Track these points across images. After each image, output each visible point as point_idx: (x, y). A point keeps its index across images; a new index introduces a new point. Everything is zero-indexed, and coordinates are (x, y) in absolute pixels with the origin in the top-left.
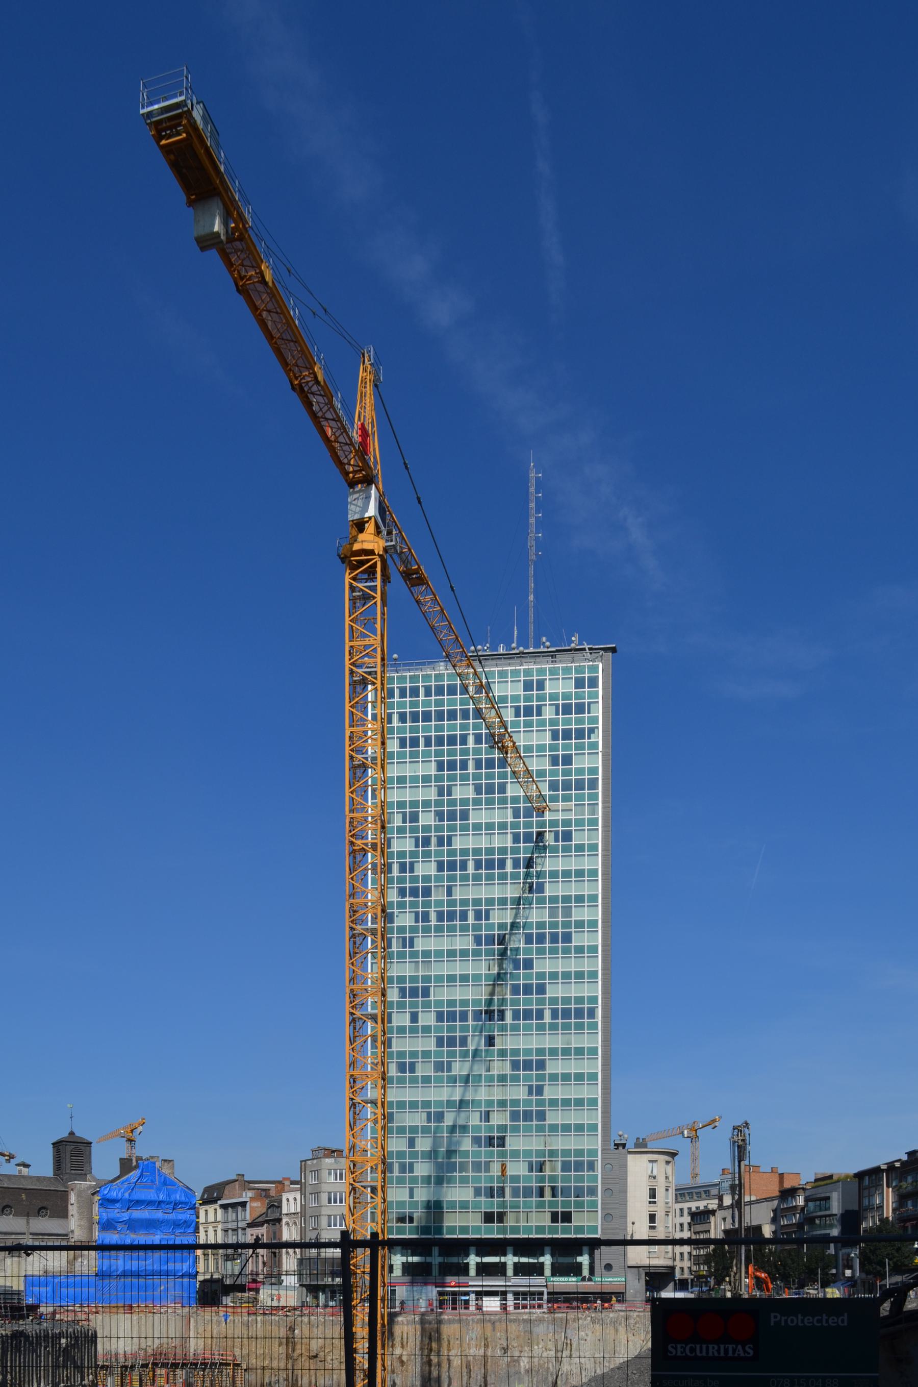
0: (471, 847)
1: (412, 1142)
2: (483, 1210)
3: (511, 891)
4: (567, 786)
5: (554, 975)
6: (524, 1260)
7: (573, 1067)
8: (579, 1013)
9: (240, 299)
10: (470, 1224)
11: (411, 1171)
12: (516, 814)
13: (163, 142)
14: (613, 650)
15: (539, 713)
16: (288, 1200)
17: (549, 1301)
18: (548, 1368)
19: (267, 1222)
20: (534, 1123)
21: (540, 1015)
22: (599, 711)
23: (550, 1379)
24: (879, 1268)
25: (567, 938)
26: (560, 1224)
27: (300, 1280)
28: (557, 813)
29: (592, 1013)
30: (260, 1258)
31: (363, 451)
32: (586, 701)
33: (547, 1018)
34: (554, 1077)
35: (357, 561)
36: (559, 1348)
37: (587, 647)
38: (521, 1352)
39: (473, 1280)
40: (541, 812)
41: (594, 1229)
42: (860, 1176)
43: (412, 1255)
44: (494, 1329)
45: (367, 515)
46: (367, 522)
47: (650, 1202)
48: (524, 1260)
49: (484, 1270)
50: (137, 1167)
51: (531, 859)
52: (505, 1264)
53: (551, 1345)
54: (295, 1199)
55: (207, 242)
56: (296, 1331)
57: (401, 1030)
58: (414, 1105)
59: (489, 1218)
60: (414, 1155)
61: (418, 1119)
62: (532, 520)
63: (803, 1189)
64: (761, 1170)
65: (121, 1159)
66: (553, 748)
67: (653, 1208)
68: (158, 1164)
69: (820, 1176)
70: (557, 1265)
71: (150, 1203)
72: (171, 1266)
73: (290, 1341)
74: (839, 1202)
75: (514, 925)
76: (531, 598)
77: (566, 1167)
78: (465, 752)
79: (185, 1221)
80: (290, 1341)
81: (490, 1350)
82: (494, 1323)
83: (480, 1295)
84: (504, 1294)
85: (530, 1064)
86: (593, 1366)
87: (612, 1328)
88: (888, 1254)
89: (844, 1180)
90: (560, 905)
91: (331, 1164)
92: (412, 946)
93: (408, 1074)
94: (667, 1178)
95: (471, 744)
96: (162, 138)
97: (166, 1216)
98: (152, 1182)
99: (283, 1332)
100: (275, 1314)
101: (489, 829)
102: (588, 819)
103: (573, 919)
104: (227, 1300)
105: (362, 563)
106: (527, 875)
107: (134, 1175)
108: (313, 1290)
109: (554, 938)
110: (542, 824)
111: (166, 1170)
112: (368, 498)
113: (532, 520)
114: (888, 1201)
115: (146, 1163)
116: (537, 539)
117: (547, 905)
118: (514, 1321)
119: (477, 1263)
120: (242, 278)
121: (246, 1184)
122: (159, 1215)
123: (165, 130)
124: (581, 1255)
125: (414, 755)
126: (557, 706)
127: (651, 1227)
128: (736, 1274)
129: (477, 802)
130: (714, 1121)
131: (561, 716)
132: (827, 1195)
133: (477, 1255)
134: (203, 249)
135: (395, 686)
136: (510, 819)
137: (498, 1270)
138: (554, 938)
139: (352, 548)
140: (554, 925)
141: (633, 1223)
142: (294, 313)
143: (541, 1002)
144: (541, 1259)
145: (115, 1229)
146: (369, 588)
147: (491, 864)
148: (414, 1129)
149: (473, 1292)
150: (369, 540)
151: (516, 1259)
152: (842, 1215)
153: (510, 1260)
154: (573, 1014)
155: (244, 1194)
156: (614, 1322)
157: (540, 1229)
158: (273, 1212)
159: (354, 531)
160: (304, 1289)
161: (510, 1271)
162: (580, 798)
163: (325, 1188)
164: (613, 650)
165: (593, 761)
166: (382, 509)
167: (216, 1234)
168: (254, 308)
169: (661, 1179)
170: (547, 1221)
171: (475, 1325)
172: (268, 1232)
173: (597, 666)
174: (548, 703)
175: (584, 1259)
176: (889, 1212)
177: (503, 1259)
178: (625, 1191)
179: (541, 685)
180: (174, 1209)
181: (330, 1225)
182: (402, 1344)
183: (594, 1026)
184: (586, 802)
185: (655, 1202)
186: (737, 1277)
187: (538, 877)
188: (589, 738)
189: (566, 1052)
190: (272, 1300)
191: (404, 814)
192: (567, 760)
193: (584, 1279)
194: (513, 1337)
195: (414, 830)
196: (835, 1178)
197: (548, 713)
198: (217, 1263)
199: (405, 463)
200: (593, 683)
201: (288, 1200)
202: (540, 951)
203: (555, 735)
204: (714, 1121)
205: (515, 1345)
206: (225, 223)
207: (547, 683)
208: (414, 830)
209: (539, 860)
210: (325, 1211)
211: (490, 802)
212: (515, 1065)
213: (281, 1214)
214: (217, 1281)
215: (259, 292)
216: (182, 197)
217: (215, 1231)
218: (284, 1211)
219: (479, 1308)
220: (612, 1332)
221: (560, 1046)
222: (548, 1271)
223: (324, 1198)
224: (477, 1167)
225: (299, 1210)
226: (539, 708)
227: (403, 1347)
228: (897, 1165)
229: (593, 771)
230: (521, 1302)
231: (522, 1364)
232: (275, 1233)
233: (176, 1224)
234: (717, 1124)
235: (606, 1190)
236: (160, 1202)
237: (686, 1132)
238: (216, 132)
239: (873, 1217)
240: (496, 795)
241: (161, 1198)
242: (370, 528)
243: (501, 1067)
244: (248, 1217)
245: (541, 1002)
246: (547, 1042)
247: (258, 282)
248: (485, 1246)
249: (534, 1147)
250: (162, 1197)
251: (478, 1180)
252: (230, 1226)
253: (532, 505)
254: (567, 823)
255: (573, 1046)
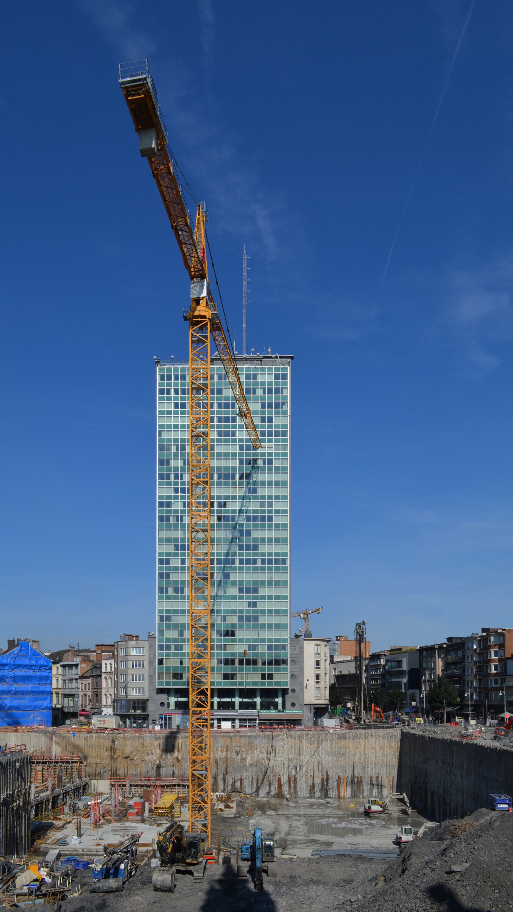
0: (216, 466)
1: (182, 633)
2: (223, 672)
3: (239, 492)
4: (270, 434)
5: (263, 540)
6: (245, 700)
7: (273, 591)
8: (277, 561)
9: (154, 180)
10: (215, 680)
11: (181, 649)
12: (241, 448)
13: (130, 98)
14: (292, 358)
15: (254, 393)
16: (106, 664)
17: (260, 724)
18: (262, 763)
19: (93, 676)
20: (252, 623)
21: (255, 562)
22: (288, 393)
23: (263, 770)
24: (440, 705)
25: (270, 519)
26: (266, 680)
27: (114, 711)
28: (266, 448)
29: (284, 561)
30: (87, 697)
31: (201, 262)
32: (281, 387)
33: (259, 564)
34: (263, 597)
35: (195, 321)
36: (269, 752)
37: (278, 355)
38: (247, 754)
39: (216, 712)
40: (255, 448)
41: (286, 683)
42: (421, 650)
43: (181, 697)
44: (231, 741)
45: (202, 296)
46: (202, 299)
47: (316, 668)
48: (245, 700)
49: (222, 706)
50: (18, 645)
51: (250, 474)
52: (234, 702)
53: (264, 750)
54: (111, 664)
55: (147, 153)
56: (116, 743)
57: (176, 569)
58: (183, 612)
59: (226, 676)
60: (183, 640)
61: (186, 620)
62: (245, 283)
63: (384, 655)
64: (349, 639)
65: (9, 641)
66: (263, 412)
67: (318, 671)
68: (30, 643)
69: (393, 648)
70: (264, 703)
71: (26, 666)
72: (37, 703)
73: (113, 749)
74: (407, 664)
75: (240, 511)
76: (245, 325)
77: (270, 648)
78: (213, 412)
79: (46, 677)
80: (113, 749)
81: (229, 753)
82: (231, 738)
83: (219, 720)
84: (233, 720)
85: (247, 589)
86: (288, 761)
87: (298, 740)
88: (445, 698)
89: (411, 652)
90: (266, 500)
91: (134, 644)
92: (182, 521)
93: (179, 594)
94: (325, 654)
95: (216, 408)
96: (129, 96)
97: (35, 674)
98: (27, 653)
99: (108, 743)
100: (103, 733)
101: (226, 456)
102: (280, 452)
103: (274, 508)
104: (68, 722)
105: (198, 323)
106: (248, 483)
107: (16, 650)
108: (123, 717)
109: (263, 519)
110: (255, 455)
111: (35, 647)
112: (202, 286)
113: (245, 283)
114: (438, 665)
115: (23, 642)
116: (248, 293)
117: (259, 500)
118: (243, 736)
119: (218, 702)
120: (156, 169)
121: (77, 652)
122: (31, 673)
123: (131, 91)
124: (277, 698)
125: (183, 413)
126: (264, 389)
127: (317, 682)
128: (358, 706)
129: (219, 441)
130: (318, 610)
131: (266, 395)
132: (400, 659)
133: (218, 697)
134: (143, 156)
135: (172, 373)
136: (238, 451)
137: (230, 706)
138: (263, 519)
139: (193, 314)
140: (263, 511)
141: (308, 680)
142: (180, 188)
143: (256, 554)
144: (255, 700)
145: (5, 682)
146: (202, 336)
147: (226, 476)
148: (183, 626)
149: (216, 718)
150: (202, 310)
151: (240, 700)
152: (409, 671)
153: (237, 700)
154: (274, 562)
155: (75, 658)
156: (300, 737)
157: (255, 683)
158: (96, 671)
159: (194, 305)
160: (119, 717)
161: (237, 707)
162: (277, 441)
163: (130, 658)
164: (292, 358)
165: (283, 420)
166: (209, 292)
167: (58, 682)
168: (160, 186)
169: (322, 655)
170: (259, 679)
171: (220, 739)
172: (92, 682)
173: (287, 368)
174: (259, 387)
175: (279, 700)
176: (439, 672)
177: (233, 700)
178: (303, 662)
179: (255, 377)
180: (39, 669)
181: (133, 680)
182: (178, 750)
183: (285, 569)
184: (281, 444)
185: (319, 668)
186: (359, 708)
187: (254, 484)
188: (282, 408)
189: (270, 583)
190: (100, 723)
191: (177, 446)
192: (270, 419)
193: (279, 711)
194: (242, 745)
195: (183, 455)
196: (404, 650)
197: (259, 393)
198: (58, 699)
199: (212, 263)
200: (285, 377)
201: (106, 664)
202: (255, 526)
203: (263, 405)
204: (318, 610)
205: (244, 750)
206: (156, 143)
207: (259, 376)
208: (183, 455)
209: (255, 475)
210: (131, 672)
211: (227, 441)
212: (241, 590)
213: (101, 672)
214: (58, 709)
215: (164, 177)
216: (133, 126)
217: (57, 680)
218: (104, 670)
219: (219, 727)
220: (299, 742)
221: (267, 580)
222: (258, 707)
223: (130, 664)
224: (220, 647)
225: (113, 670)
226: (254, 390)
227: (179, 751)
228: (445, 646)
229: (285, 426)
230: (243, 724)
231: (247, 761)
232: (97, 683)
233: (41, 678)
234: (320, 611)
235: (292, 661)
236: (31, 666)
237: (302, 615)
238: (156, 93)
239: (430, 674)
240: (230, 437)
241: (32, 664)
242: (203, 303)
243: (233, 591)
244: (79, 673)
245: (256, 554)
246: (260, 577)
247: (166, 172)
248: (223, 693)
249: (252, 637)
250: (33, 663)
251: (219, 654)
252: (67, 677)
253: (245, 274)
254: (270, 454)
255: (274, 580)
